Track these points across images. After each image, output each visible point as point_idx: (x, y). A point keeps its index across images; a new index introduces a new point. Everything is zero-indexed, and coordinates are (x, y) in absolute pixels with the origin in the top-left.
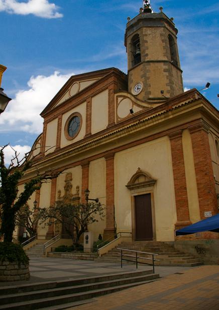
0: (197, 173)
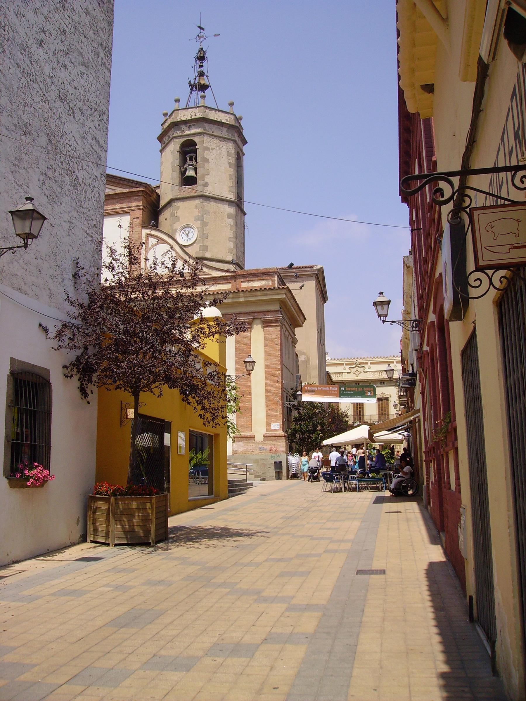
0: (266, 377)
